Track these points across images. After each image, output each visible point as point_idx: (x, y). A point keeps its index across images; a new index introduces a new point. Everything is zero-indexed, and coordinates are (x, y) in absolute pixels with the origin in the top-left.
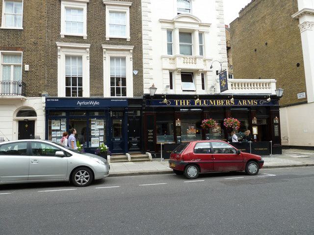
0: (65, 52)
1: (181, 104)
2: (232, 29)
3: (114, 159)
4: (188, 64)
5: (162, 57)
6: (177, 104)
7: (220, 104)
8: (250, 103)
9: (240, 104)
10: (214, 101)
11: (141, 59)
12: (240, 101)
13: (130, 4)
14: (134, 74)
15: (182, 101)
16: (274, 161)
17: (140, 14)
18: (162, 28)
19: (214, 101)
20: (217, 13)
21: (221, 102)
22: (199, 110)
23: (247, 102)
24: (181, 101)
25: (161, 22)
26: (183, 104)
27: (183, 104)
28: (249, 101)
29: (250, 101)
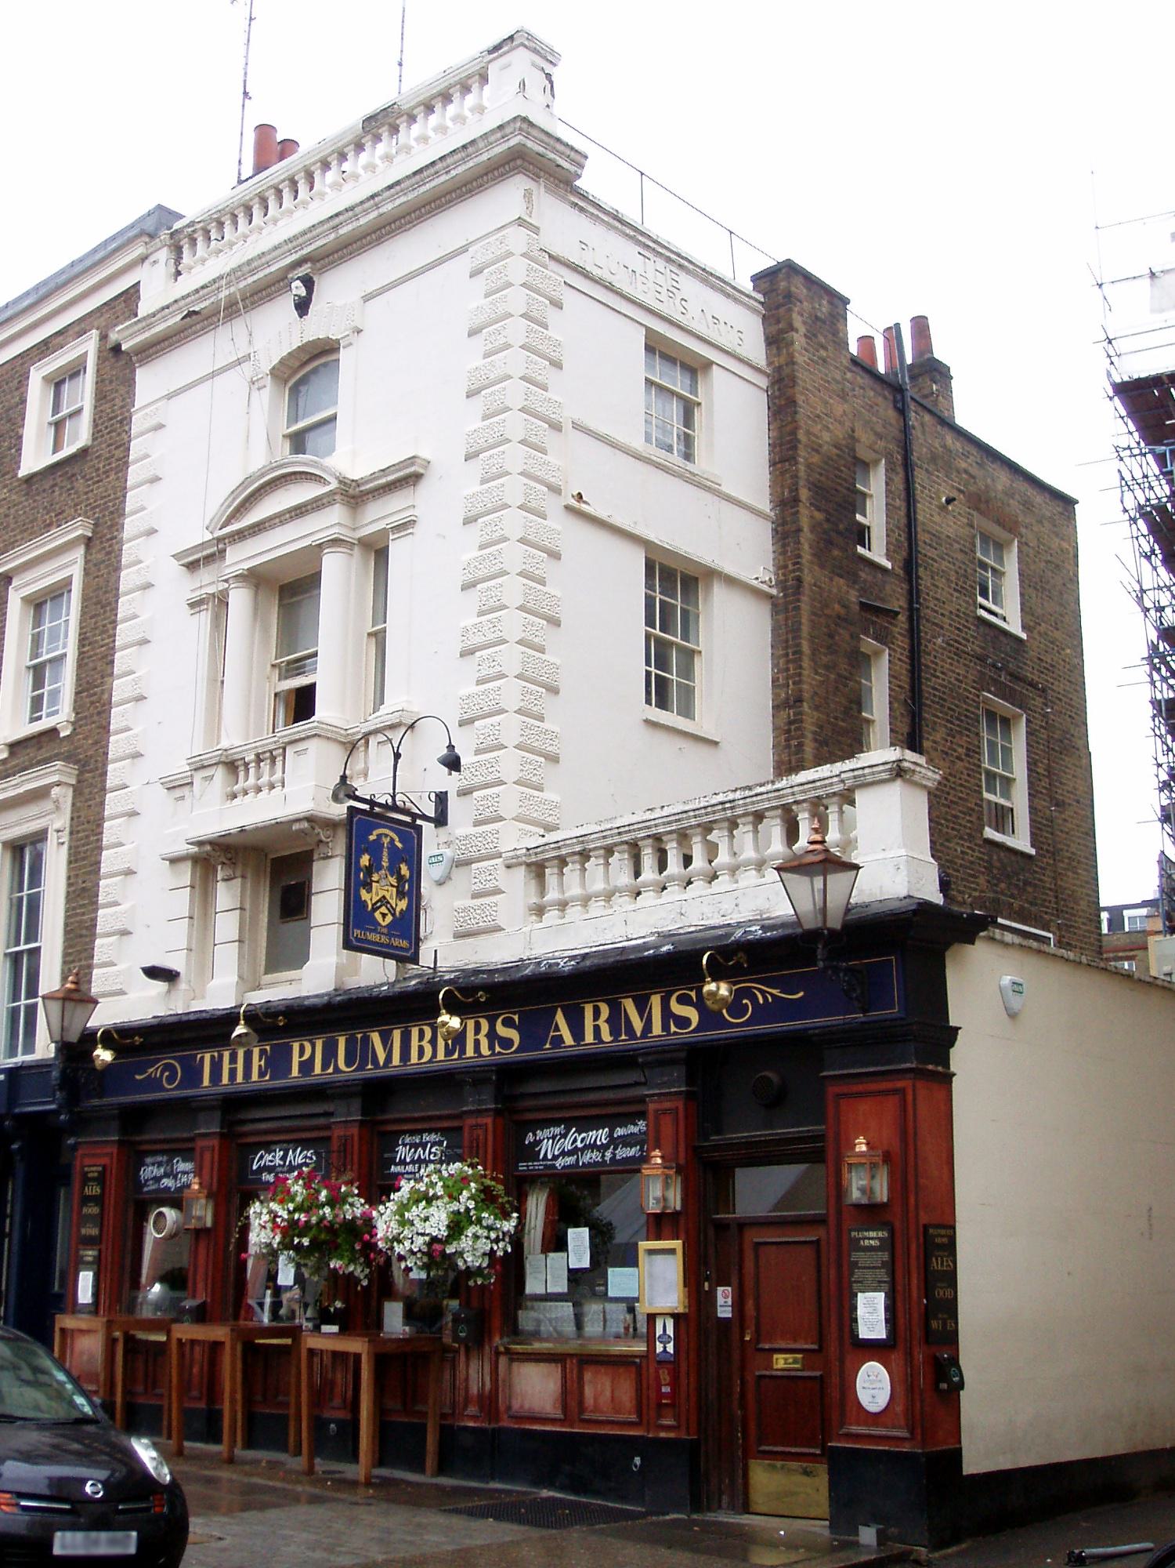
0: (995, 614)
1: (225, 1080)
3: (573, 161)
6: (206, 1082)
8: (638, 1025)
9: (559, 1040)
10: (397, 1035)
12: (560, 1018)
16: (869, 1239)
19: (397, 1035)
22: (3, 1288)
23: (617, 1020)
27: (233, 1073)
28: (629, 1005)
29: (642, 1006)
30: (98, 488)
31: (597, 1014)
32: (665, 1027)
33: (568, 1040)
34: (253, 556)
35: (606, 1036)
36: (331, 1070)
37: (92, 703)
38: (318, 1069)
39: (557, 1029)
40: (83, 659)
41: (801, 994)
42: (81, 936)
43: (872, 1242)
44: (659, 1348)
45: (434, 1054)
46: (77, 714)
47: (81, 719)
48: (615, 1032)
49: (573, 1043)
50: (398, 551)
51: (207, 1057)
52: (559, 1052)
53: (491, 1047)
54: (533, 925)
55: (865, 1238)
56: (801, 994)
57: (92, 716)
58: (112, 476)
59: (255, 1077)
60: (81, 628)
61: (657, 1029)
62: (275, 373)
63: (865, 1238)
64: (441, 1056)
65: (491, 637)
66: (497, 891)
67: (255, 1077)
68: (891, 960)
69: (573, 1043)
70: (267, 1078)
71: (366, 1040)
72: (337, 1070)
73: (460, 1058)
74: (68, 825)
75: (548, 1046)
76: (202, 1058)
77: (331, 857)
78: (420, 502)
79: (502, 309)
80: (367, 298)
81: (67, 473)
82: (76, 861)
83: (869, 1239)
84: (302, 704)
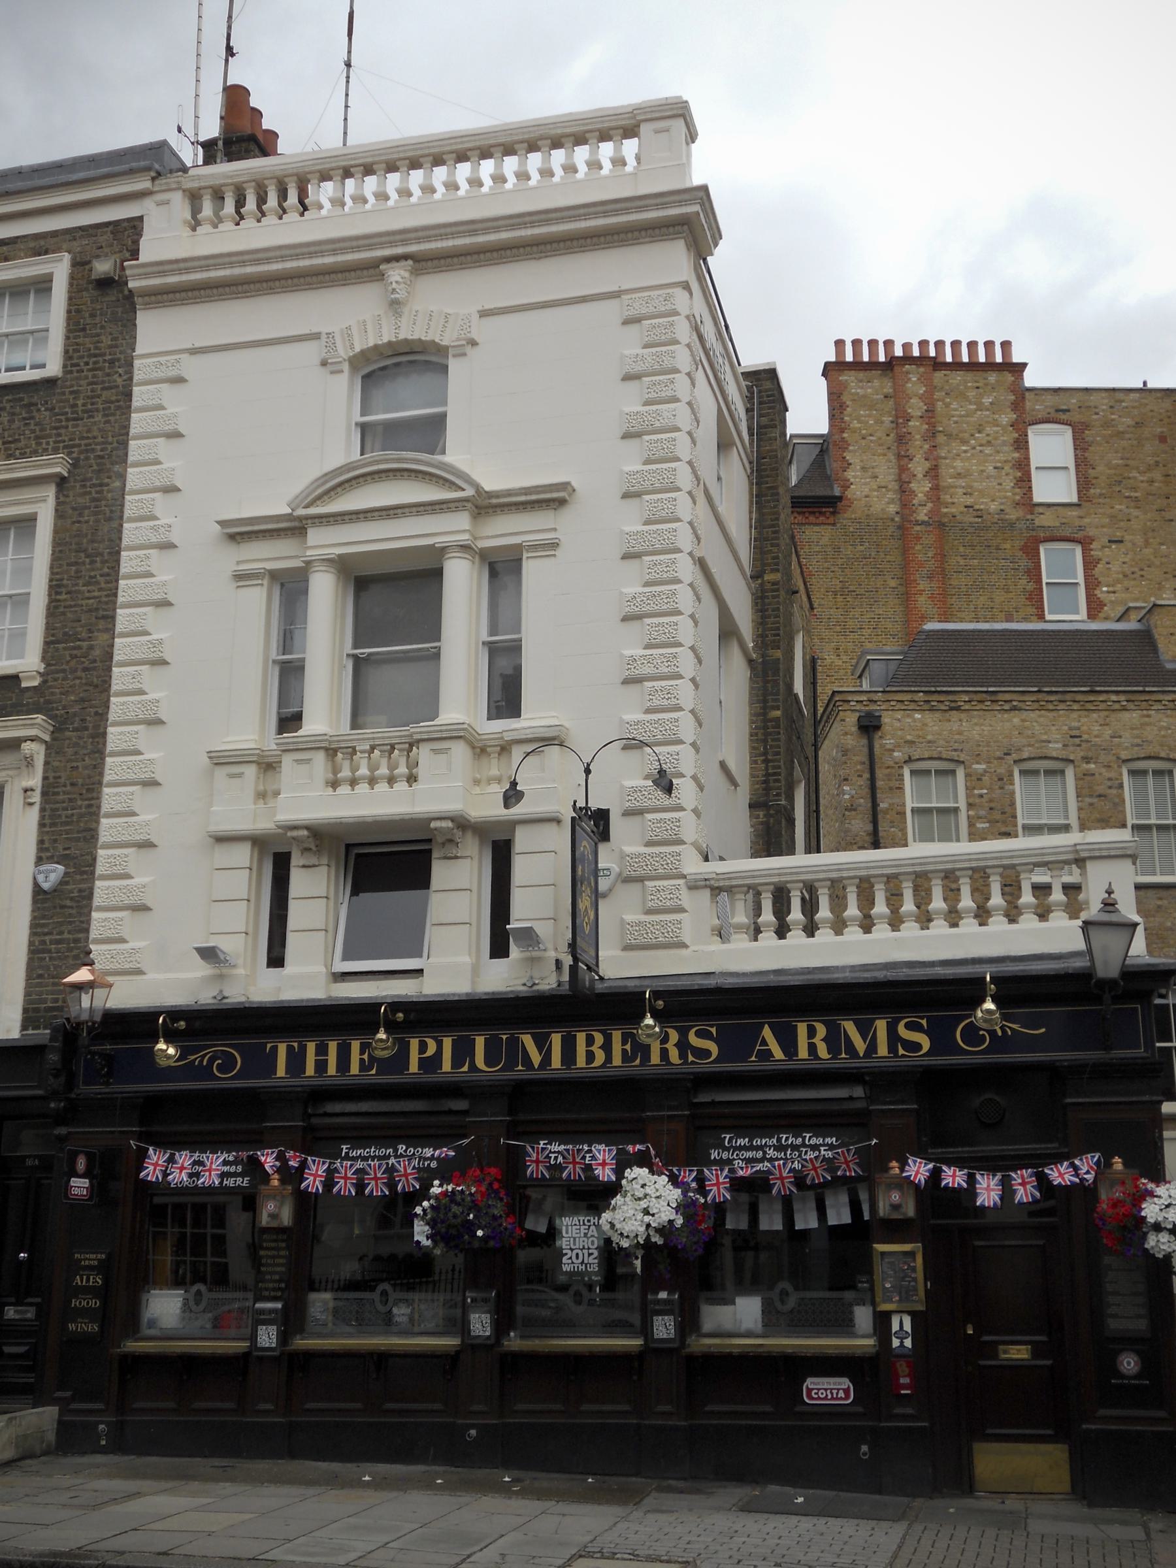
1: (310, 1070)
2: (1090, 1505)
4: (382, 787)
5: (219, 760)
6: (281, 1071)
7: (600, 1057)
9: (767, 1055)
10: (556, 1040)
11: (92, 787)
12: (767, 1032)
13: (57, 465)
14: (37, 890)
15: (322, 1050)
16: (89, 1260)
17: (114, 515)
18: (239, 577)
19: (556, 1040)
20: (630, 401)
21: (607, 1047)
23: (835, 1039)
24: (311, 1047)
25: (233, 537)
26: (321, 1066)
27: (321, 1066)
28: (850, 1027)
29: (865, 1029)
30: (77, 426)
31: (812, 1032)
32: (892, 1048)
33: (778, 1054)
34: (254, 561)
35: (823, 1051)
36: (465, 1069)
37: (73, 657)
38: (447, 1066)
39: (764, 1043)
40: (56, 607)
41: (1043, 1030)
42: (63, 907)
43: (92, 1262)
44: (896, 1343)
45: (609, 1058)
46: (48, 665)
47: (53, 672)
48: (833, 1049)
49: (783, 1057)
50: (531, 568)
51: (282, 1049)
52: (767, 1066)
53: (683, 1056)
54: (716, 946)
55: (86, 1259)
56: (1043, 1030)
57: (74, 671)
58: (99, 417)
59: (355, 1069)
60: (52, 573)
61: (883, 1050)
62: (358, 361)
63: (86, 1259)
64: (617, 1060)
65: (665, 670)
66: (682, 910)
67: (355, 1069)
68: (1136, 1009)
69: (783, 1057)
70: (373, 1072)
71: (514, 1042)
72: (473, 1068)
73: (642, 1064)
74: (40, 784)
75: (753, 1058)
76: (275, 1050)
77: (456, 857)
78: (562, 524)
79: (667, 363)
80: (484, 314)
81: (21, 399)
82: (53, 825)
83: (89, 1260)
84: (289, 721)
